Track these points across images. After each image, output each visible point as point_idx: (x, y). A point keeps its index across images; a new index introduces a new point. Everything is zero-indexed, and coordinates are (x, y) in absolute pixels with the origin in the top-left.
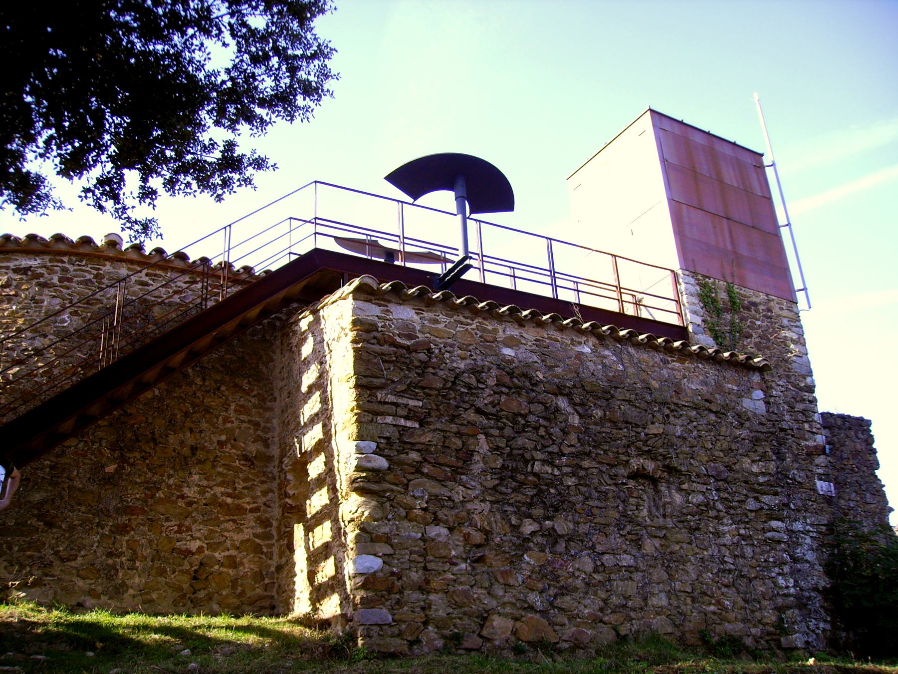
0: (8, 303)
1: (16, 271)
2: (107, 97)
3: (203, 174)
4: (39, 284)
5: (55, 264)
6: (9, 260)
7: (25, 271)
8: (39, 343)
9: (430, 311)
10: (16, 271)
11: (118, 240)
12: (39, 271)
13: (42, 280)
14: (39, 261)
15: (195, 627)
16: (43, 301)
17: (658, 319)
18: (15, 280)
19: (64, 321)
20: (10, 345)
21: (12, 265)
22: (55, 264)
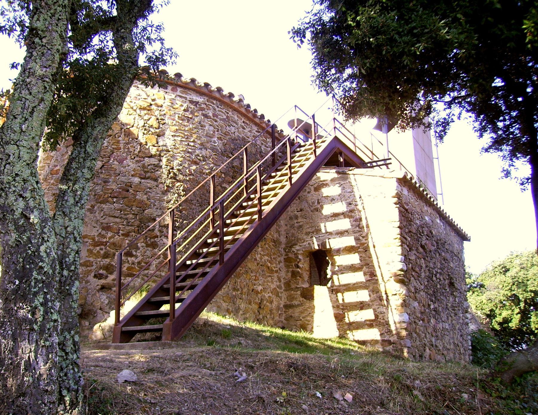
0: (188, 122)
1: (191, 102)
2: (356, 67)
3: (322, 77)
4: (204, 115)
5: (210, 104)
6: (187, 94)
7: (196, 103)
8: (204, 152)
9: (178, 346)
10: (191, 102)
11: (242, 99)
12: (203, 106)
13: (204, 112)
14: (202, 100)
15: (262, 331)
16: (205, 126)
17: (357, 153)
18: (191, 108)
19: (215, 142)
20: (190, 150)
21: (188, 97)
22: (210, 104)
